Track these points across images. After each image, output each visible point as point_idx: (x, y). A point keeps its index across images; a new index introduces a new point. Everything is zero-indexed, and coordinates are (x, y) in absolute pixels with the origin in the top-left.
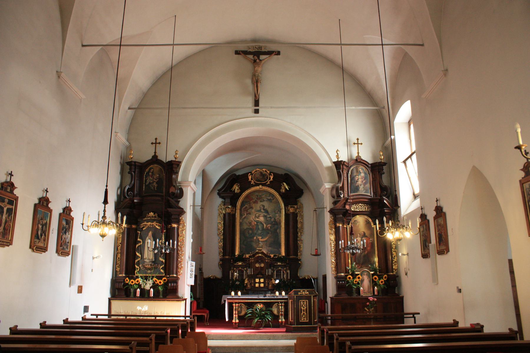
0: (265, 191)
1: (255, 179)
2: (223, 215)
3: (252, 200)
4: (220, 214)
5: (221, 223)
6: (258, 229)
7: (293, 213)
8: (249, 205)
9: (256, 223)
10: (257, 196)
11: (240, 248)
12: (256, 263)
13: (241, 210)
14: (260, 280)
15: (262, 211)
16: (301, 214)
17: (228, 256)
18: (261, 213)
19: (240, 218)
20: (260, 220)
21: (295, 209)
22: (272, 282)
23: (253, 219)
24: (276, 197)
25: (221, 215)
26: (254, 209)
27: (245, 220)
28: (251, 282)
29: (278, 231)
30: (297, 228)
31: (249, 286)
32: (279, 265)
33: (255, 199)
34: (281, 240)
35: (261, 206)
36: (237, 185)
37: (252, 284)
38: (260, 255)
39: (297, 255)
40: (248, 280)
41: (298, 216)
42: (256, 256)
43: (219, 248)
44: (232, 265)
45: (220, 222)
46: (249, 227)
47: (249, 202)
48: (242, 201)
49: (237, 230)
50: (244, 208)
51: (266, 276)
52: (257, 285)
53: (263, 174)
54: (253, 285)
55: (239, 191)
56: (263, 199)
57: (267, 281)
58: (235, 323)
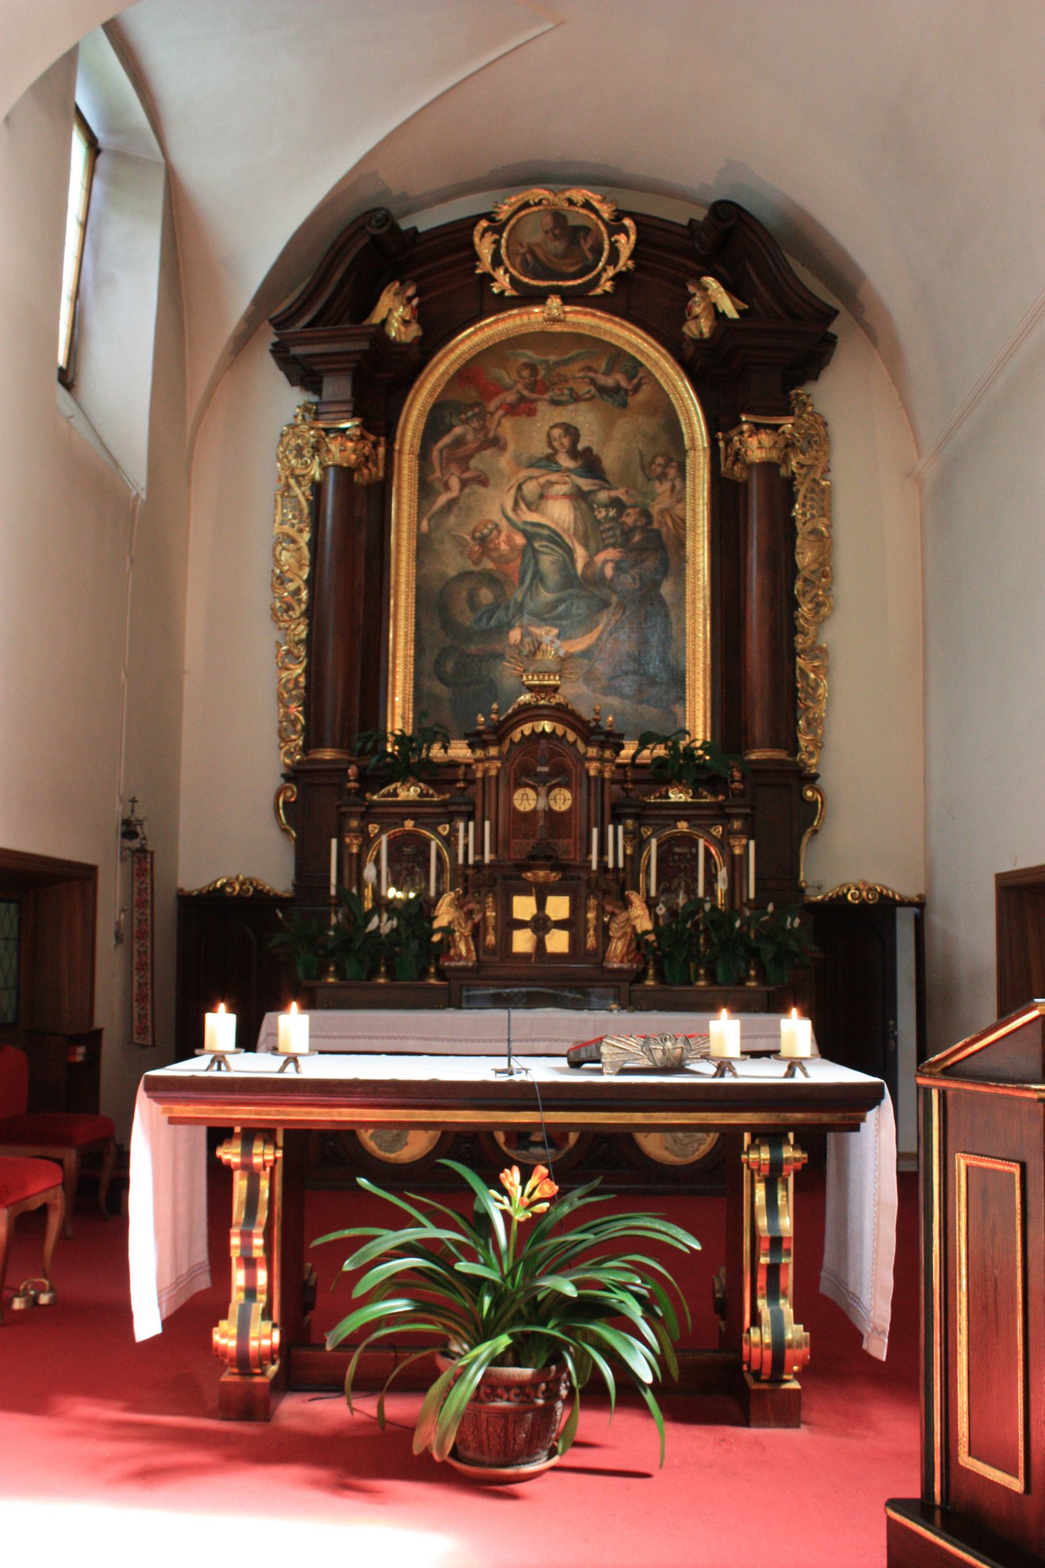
0: (579, 339)
1: (518, 261)
2: (307, 488)
3: (496, 394)
4: (288, 487)
5: (294, 541)
6: (538, 577)
7: (769, 468)
8: (475, 425)
9: (520, 540)
10: (533, 368)
11: (420, 697)
12: (519, 785)
13: (424, 456)
14: (541, 905)
15: (565, 461)
16: (816, 482)
17: (333, 746)
18: (554, 477)
19: (420, 507)
20: (552, 520)
21: (782, 443)
22: (628, 919)
23: (505, 515)
24: (649, 373)
25: (297, 491)
26: (511, 447)
27: (452, 520)
28: (477, 918)
29: (666, 589)
30: (793, 571)
31: (463, 948)
32: (677, 805)
33: (520, 387)
34: (689, 651)
35: (557, 432)
36: (396, 294)
37: (486, 934)
38: (548, 730)
39: (794, 748)
40: (459, 903)
41: (800, 498)
42: (516, 736)
43: (280, 699)
44: (355, 805)
45: (292, 532)
46: (476, 563)
47: (477, 404)
48: (432, 401)
49: (397, 582)
50: (447, 446)
51: (584, 875)
52: (522, 942)
53: (572, 222)
54: (491, 939)
55: (414, 331)
56: (571, 390)
57: (591, 915)
58: (244, 1362)
